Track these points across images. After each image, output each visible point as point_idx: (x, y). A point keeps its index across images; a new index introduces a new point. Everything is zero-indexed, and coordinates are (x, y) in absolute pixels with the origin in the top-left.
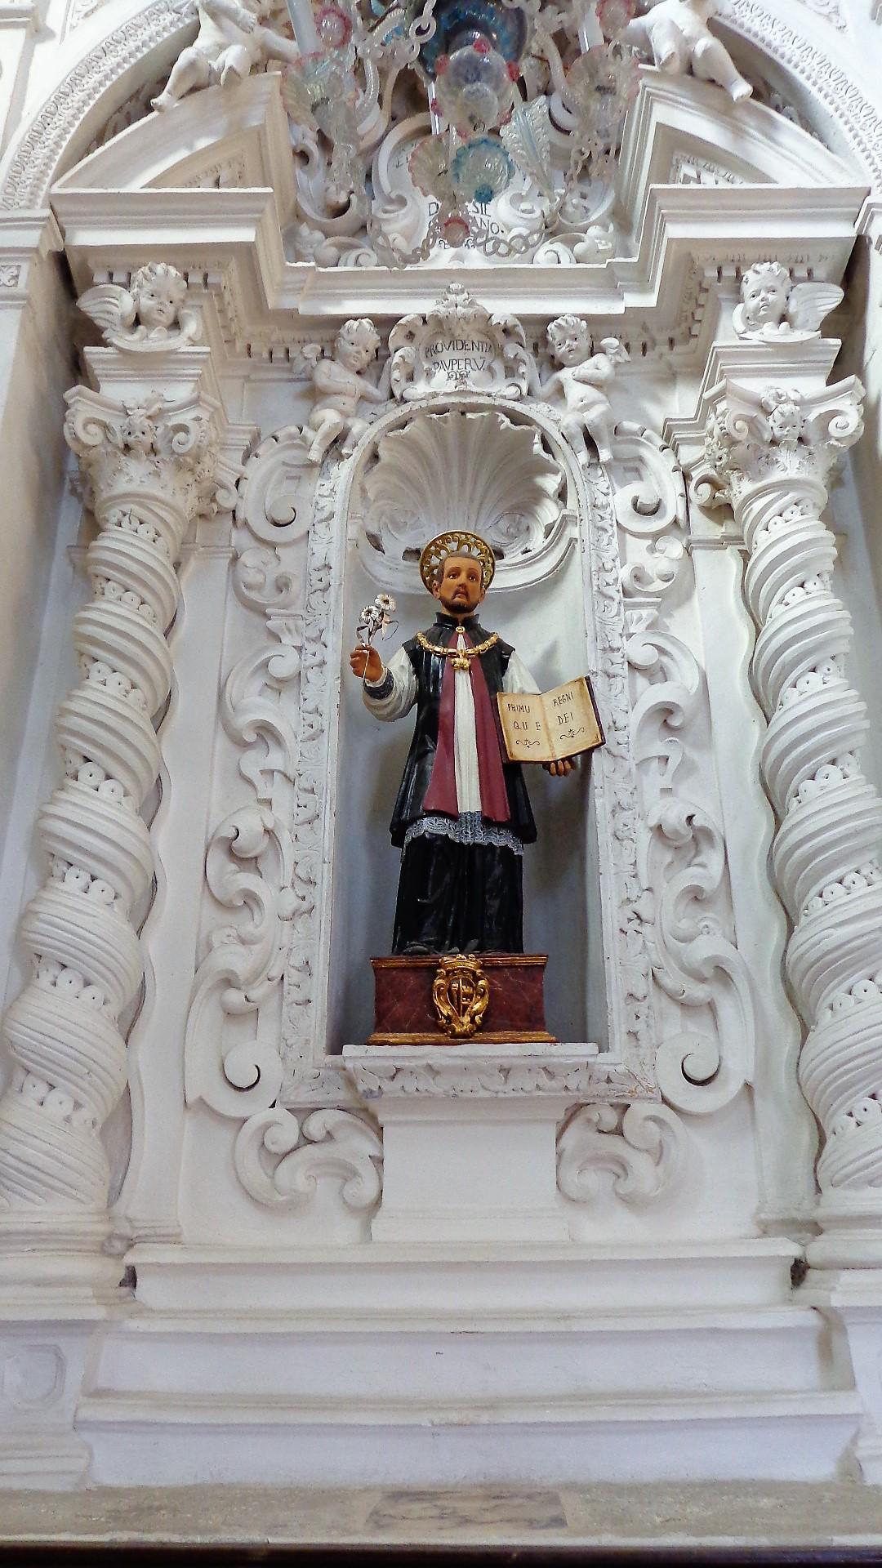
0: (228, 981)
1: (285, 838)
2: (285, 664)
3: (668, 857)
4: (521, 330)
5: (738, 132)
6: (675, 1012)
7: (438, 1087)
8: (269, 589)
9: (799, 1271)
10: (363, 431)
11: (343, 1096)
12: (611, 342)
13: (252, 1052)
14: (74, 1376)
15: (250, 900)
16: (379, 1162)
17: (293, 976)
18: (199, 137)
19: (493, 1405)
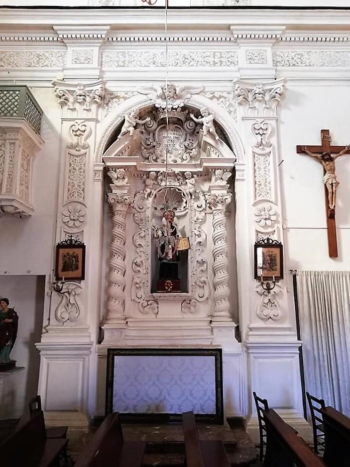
0: (137, 283)
1: (144, 262)
2: (143, 234)
3: (199, 265)
4: (180, 174)
5: (217, 143)
6: (199, 288)
7: (166, 298)
8: (139, 220)
9: (211, 322)
10: (154, 192)
11: (153, 299)
12: (195, 176)
13: (141, 293)
14: (123, 333)
15: (139, 271)
16: (158, 307)
17: (145, 283)
18: (125, 142)
19: (172, 337)
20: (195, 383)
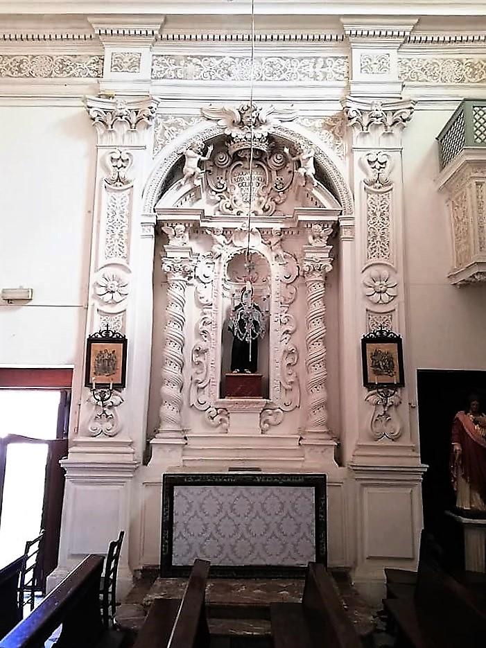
20: (222, 514)
